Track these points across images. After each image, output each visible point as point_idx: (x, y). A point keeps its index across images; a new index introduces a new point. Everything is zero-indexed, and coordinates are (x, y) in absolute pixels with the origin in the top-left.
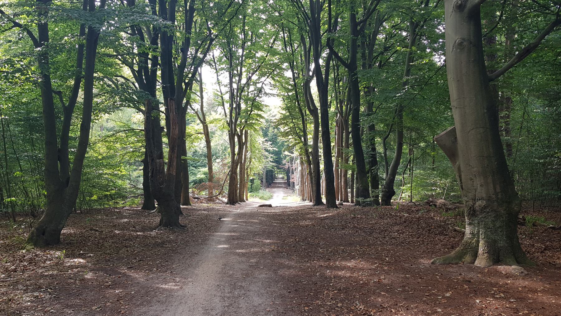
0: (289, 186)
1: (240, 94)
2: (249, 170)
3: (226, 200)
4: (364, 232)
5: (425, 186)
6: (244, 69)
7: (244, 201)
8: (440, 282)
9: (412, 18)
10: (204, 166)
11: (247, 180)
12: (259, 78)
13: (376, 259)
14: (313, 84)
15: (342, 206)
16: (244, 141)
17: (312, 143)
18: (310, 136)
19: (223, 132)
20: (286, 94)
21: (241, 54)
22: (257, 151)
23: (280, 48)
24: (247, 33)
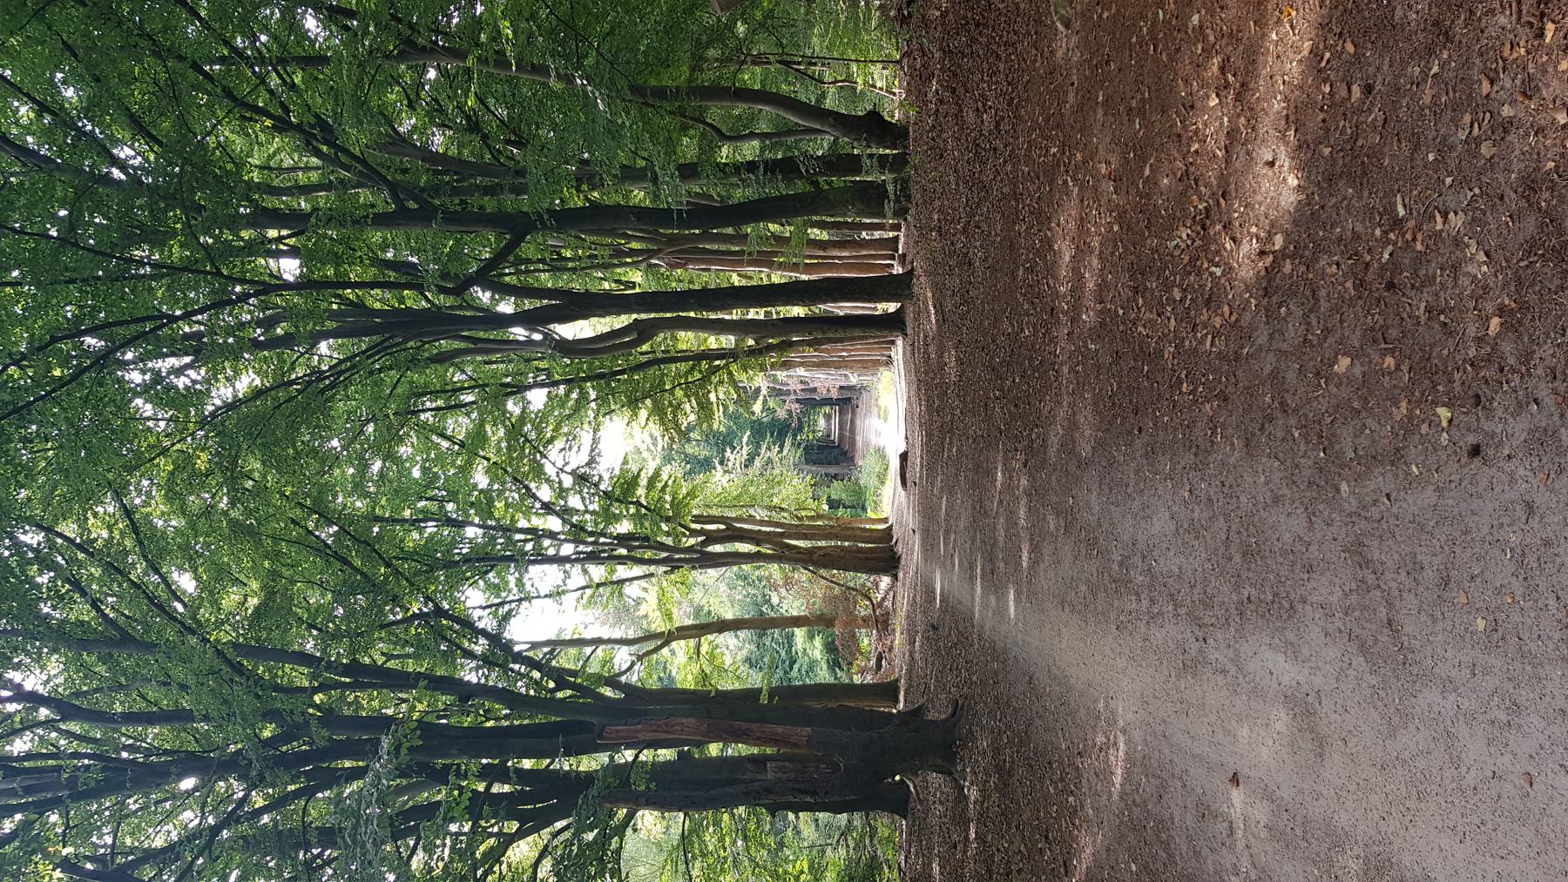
0: (849, 399)
1: (591, 534)
3: (885, 581)
4: (978, 205)
5: (856, 25)
6: (523, 524)
8: (1118, 11)
9: (388, 56)
10: (790, 638)
12: (548, 480)
13: (1053, 180)
14: (570, 331)
15: (909, 258)
16: (722, 527)
17: (732, 338)
18: (713, 342)
19: (695, 583)
20: (593, 405)
21: (480, 532)
22: (752, 489)
23: (464, 420)
24: (422, 511)
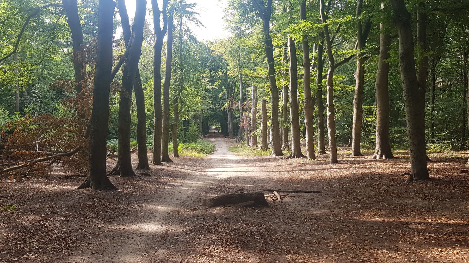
7: (169, 161)
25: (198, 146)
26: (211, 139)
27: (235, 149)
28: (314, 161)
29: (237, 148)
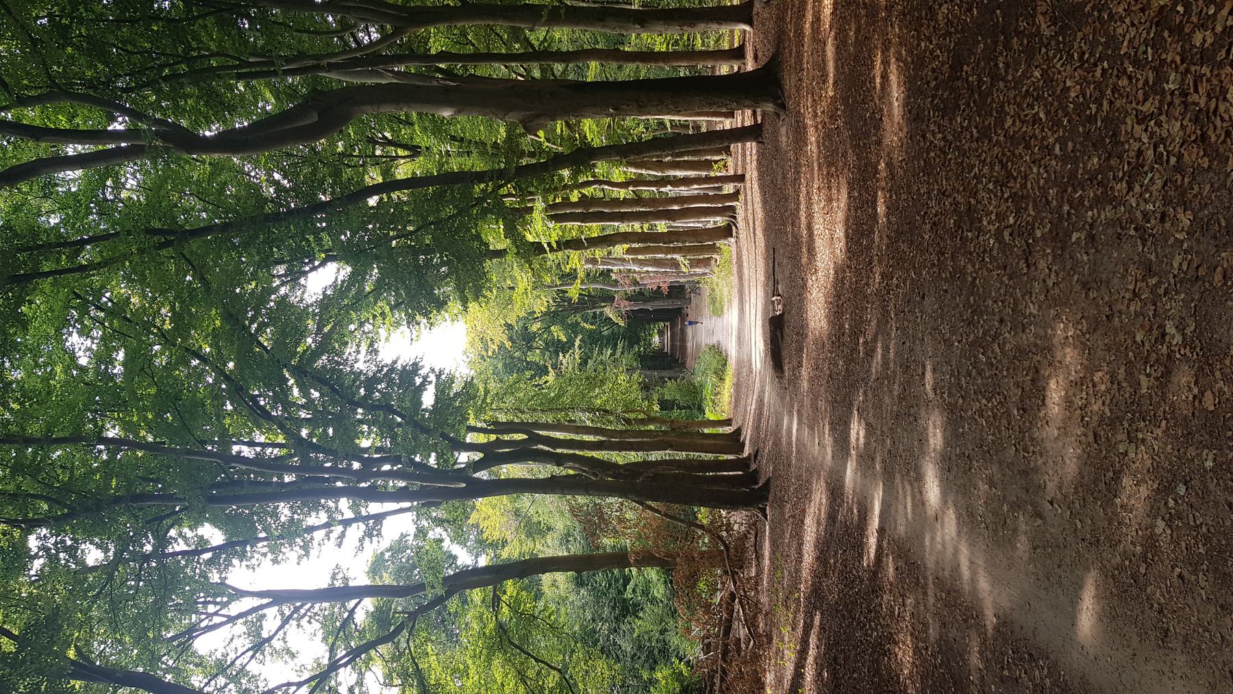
2: (632, 416)
7: (738, 432)
11: (662, 422)
25: (711, 380)
26: (689, 350)
27: (717, 305)
28: (741, 197)
29: (713, 301)
